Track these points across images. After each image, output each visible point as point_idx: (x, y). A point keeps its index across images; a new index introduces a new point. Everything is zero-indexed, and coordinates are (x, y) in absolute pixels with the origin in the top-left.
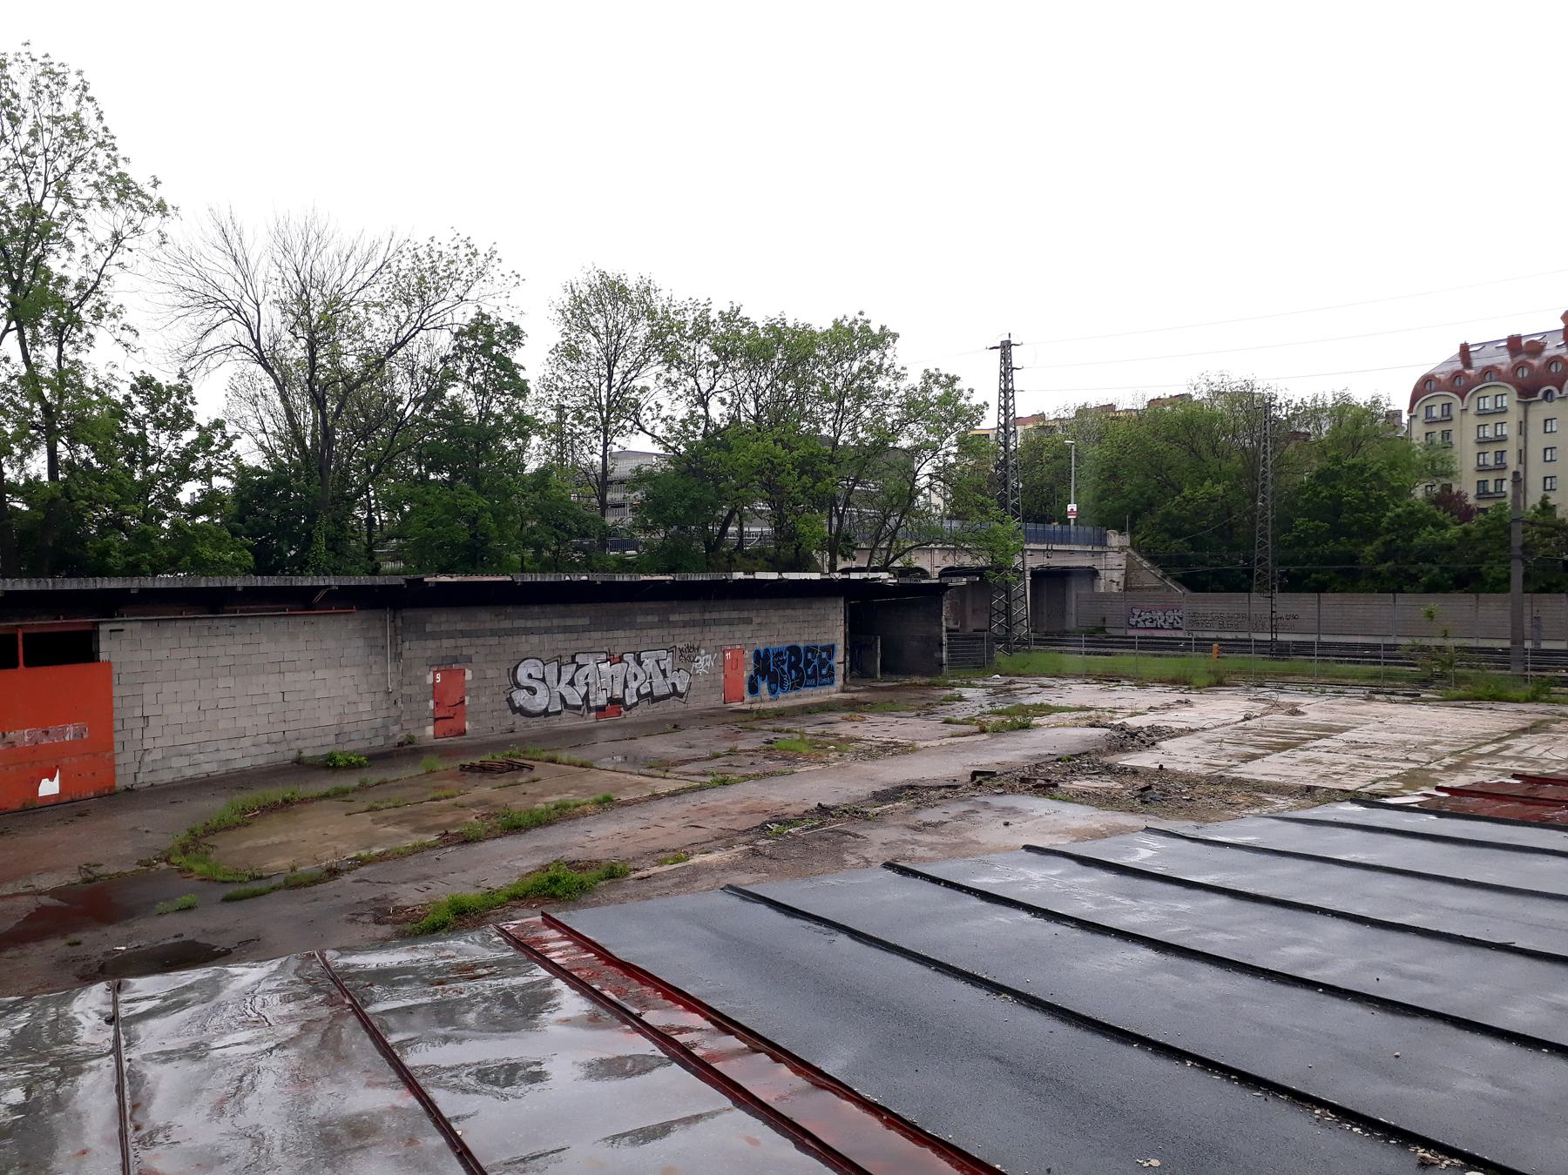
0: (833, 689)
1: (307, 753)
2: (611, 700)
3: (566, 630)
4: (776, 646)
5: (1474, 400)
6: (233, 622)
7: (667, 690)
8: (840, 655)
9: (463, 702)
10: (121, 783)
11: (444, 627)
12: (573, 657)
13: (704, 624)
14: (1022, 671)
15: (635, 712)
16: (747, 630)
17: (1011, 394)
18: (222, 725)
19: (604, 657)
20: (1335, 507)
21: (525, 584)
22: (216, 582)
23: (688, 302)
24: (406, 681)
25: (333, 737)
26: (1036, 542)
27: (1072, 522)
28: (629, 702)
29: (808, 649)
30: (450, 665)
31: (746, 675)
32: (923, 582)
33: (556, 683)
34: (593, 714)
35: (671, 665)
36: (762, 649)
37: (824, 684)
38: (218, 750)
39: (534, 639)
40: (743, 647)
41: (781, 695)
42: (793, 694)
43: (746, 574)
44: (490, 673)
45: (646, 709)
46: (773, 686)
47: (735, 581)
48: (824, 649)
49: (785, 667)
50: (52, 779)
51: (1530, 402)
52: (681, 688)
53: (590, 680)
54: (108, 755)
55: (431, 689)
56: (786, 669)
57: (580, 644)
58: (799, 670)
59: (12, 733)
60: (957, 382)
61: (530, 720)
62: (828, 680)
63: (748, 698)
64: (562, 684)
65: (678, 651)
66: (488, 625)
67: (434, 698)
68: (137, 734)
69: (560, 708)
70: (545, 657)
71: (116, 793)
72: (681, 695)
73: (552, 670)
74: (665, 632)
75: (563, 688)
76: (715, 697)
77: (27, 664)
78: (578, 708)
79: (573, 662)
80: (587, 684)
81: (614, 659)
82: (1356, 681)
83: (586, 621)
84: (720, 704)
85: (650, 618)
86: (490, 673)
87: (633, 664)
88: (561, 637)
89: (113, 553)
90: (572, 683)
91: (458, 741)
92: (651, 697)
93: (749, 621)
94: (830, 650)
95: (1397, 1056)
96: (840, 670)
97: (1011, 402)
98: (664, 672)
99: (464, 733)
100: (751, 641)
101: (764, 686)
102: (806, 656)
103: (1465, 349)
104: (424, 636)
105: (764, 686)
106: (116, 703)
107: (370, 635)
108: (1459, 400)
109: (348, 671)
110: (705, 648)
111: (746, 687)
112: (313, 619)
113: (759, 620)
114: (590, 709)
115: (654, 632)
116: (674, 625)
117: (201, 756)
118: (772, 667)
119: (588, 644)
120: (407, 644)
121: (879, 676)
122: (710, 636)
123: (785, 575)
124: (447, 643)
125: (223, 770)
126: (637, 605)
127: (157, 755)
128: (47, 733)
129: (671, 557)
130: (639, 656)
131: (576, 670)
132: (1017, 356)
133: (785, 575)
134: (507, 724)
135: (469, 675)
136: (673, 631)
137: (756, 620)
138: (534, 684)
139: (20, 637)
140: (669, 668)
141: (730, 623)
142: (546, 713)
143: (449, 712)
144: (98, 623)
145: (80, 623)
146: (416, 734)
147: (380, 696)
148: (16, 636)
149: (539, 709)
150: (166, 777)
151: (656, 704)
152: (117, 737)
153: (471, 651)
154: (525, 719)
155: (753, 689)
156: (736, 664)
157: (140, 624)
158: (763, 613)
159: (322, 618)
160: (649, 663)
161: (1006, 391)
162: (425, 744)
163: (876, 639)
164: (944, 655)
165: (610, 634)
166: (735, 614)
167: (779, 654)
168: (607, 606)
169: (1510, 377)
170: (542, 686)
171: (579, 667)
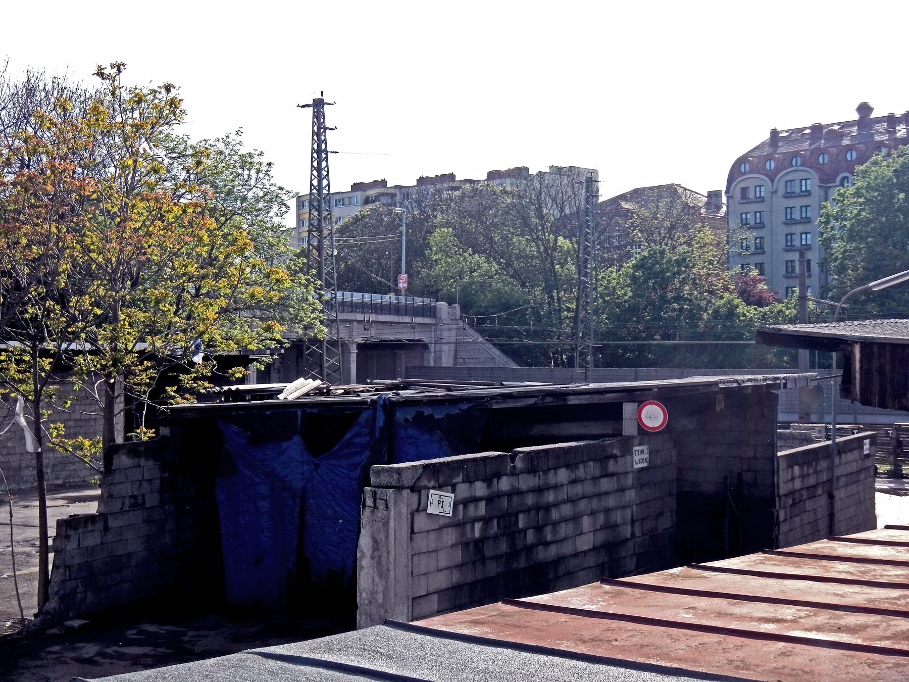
5: (782, 183)
17: (324, 156)
20: (761, 297)
51: (830, 187)
60: (181, 103)
82: (776, 563)
97: (324, 164)
103: (774, 133)
108: (769, 182)
161: (319, 151)
169: (809, 161)
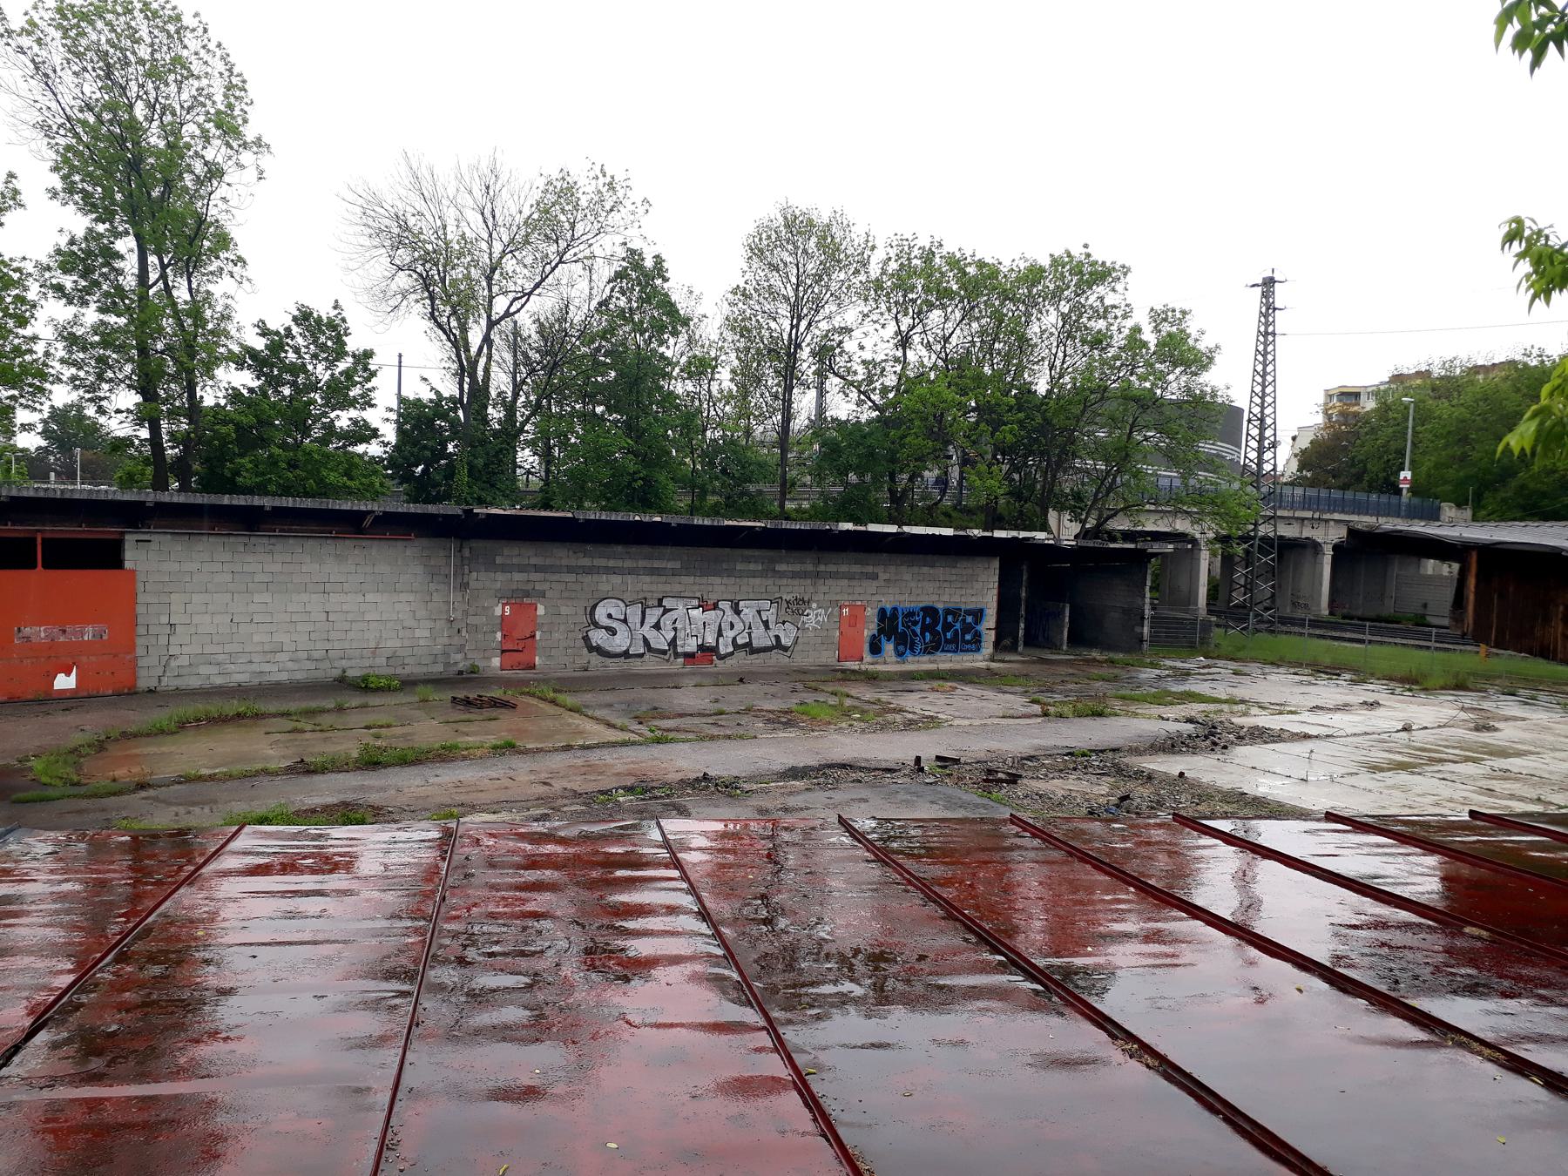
0: (978, 656)
1: (351, 673)
2: (701, 647)
3: (653, 572)
4: (907, 605)
6: (273, 540)
7: (768, 642)
8: (990, 621)
9: (534, 636)
10: (143, 683)
11: (515, 561)
12: (660, 601)
13: (818, 575)
14: (1240, 655)
15: (729, 662)
16: (871, 586)
18: (256, 638)
19: (695, 602)
21: (588, 521)
22: (240, 500)
23: (894, 238)
24: (471, 611)
25: (384, 660)
26: (1343, 512)
27: (1404, 492)
28: (722, 651)
29: (948, 611)
30: (521, 599)
31: (866, 633)
32: (1112, 546)
33: (638, 625)
34: (681, 660)
35: (774, 617)
36: (888, 607)
37: (967, 651)
38: (250, 662)
39: (616, 579)
40: (865, 603)
41: (910, 658)
42: (926, 658)
43: (856, 524)
44: (564, 610)
45: (741, 661)
46: (901, 648)
47: (841, 531)
48: (968, 612)
49: (918, 629)
50: (68, 674)
52: (785, 641)
53: (678, 625)
54: (128, 657)
55: (499, 621)
56: (918, 631)
57: (667, 588)
58: (934, 633)
59: (28, 629)
61: (609, 661)
62: (974, 647)
63: (868, 657)
64: (646, 627)
65: (784, 605)
66: (565, 562)
67: (502, 630)
68: (163, 640)
69: (642, 651)
70: (628, 597)
71: (136, 693)
72: (786, 649)
73: (634, 613)
74: (770, 582)
75: (647, 631)
76: (826, 654)
77: (46, 566)
78: (664, 652)
79: (660, 605)
80: (675, 629)
81: (704, 606)
83: (677, 565)
84: (832, 661)
85: (752, 567)
86: (564, 610)
87: (729, 612)
88: (647, 579)
89: (244, 474)
90: (657, 626)
91: (522, 674)
92: (749, 648)
93: (875, 577)
94: (978, 614)
95: (402, 1171)
96: (989, 638)
98: (766, 624)
99: (533, 667)
100: (877, 598)
101: (889, 647)
102: (945, 619)
104: (491, 566)
105: (889, 647)
106: (140, 609)
107: (432, 563)
109: (404, 597)
110: (817, 602)
111: (866, 647)
112: (364, 543)
113: (887, 576)
114: (677, 655)
115: (757, 581)
116: (782, 575)
117: (232, 666)
118: (900, 627)
119: (677, 588)
120: (474, 574)
121: (1065, 648)
122: (824, 589)
123: (906, 529)
124: (517, 576)
125: (256, 681)
126: (738, 552)
127: (184, 661)
128: (64, 631)
129: (852, 506)
130: (737, 604)
131: (663, 615)
132: (1281, 295)
133: (906, 529)
134: (581, 662)
135: (541, 610)
136: (779, 582)
137: (883, 576)
138: (615, 625)
139: (39, 541)
140: (772, 619)
141: (851, 577)
142: (626, 654)
143: (518, 646)
144: (123, 533)
145: (109, 531)
146: (481, 664)
147: (441, 624)
148: (35, 539)
149: (618, 650)
150: (194, 683)
151: (755, 656)
152: (140, 641)
153: (546, 586)
154: (603, 659)
155: (875, 649)
156: (854, 620)
157: (169, 536)
158: (892, 569)
159: (376, 542)
160: (748, 611)
162: (489, 674)
163: (1064, 607)
164: (1146, 630)
165: (704, 580)
166: (856, 569)
167: (911, 614)
168: (705, 551)
170: (624, 627)
171: (666, 611)
